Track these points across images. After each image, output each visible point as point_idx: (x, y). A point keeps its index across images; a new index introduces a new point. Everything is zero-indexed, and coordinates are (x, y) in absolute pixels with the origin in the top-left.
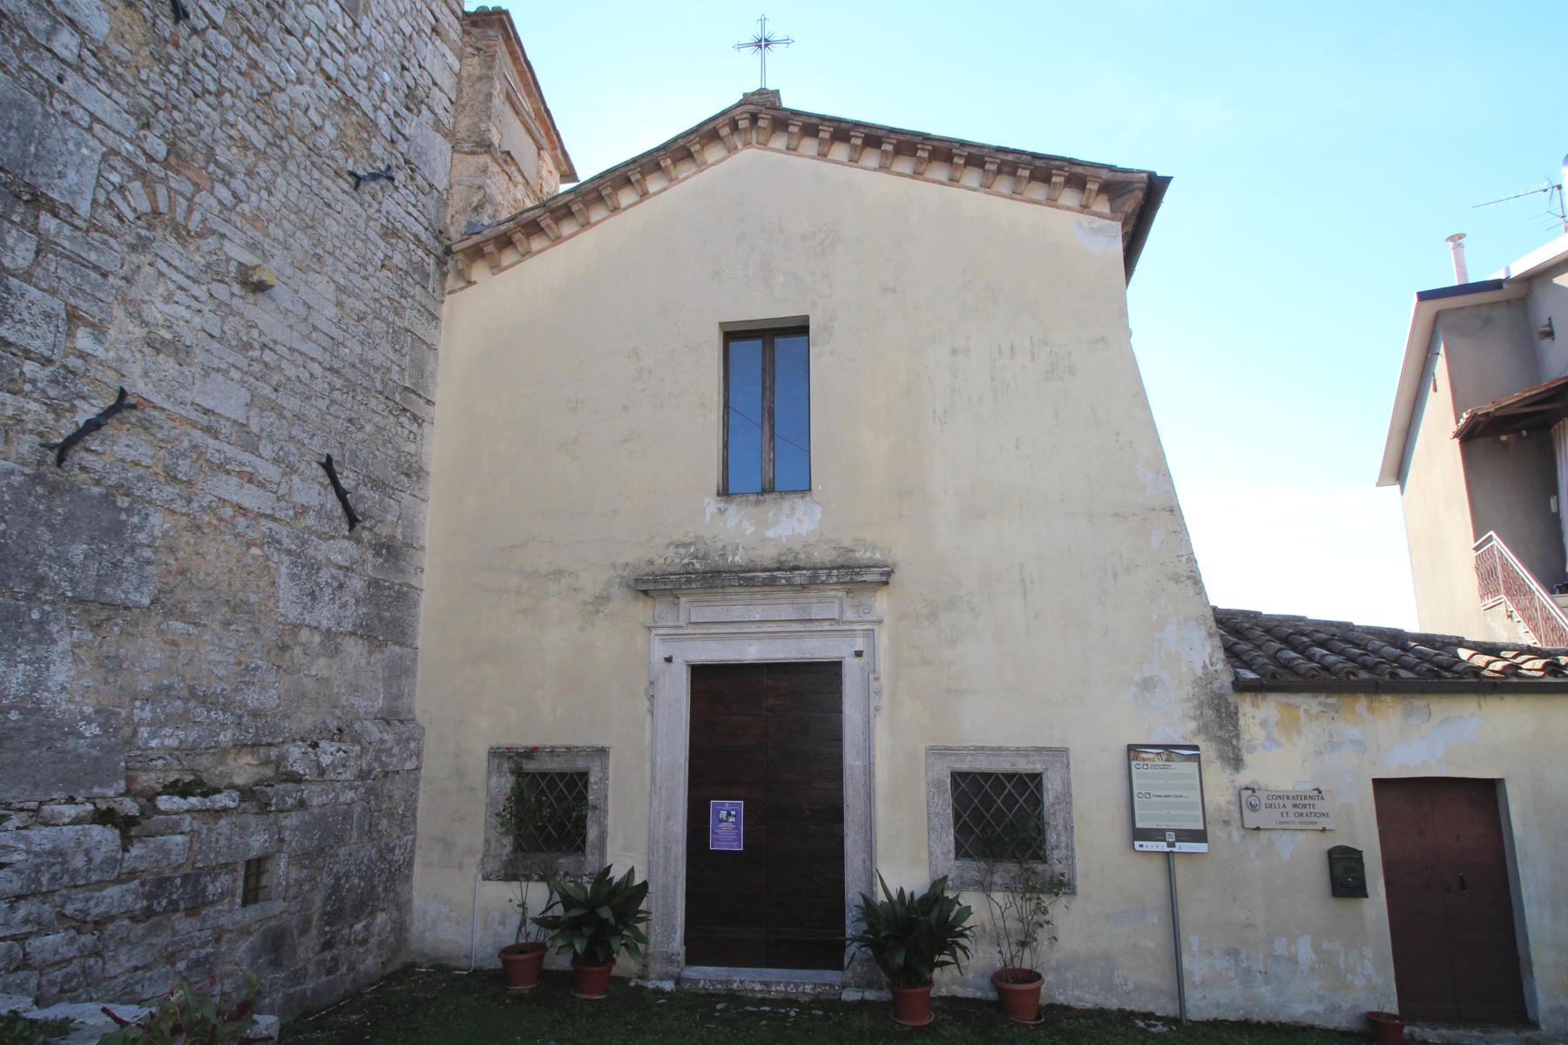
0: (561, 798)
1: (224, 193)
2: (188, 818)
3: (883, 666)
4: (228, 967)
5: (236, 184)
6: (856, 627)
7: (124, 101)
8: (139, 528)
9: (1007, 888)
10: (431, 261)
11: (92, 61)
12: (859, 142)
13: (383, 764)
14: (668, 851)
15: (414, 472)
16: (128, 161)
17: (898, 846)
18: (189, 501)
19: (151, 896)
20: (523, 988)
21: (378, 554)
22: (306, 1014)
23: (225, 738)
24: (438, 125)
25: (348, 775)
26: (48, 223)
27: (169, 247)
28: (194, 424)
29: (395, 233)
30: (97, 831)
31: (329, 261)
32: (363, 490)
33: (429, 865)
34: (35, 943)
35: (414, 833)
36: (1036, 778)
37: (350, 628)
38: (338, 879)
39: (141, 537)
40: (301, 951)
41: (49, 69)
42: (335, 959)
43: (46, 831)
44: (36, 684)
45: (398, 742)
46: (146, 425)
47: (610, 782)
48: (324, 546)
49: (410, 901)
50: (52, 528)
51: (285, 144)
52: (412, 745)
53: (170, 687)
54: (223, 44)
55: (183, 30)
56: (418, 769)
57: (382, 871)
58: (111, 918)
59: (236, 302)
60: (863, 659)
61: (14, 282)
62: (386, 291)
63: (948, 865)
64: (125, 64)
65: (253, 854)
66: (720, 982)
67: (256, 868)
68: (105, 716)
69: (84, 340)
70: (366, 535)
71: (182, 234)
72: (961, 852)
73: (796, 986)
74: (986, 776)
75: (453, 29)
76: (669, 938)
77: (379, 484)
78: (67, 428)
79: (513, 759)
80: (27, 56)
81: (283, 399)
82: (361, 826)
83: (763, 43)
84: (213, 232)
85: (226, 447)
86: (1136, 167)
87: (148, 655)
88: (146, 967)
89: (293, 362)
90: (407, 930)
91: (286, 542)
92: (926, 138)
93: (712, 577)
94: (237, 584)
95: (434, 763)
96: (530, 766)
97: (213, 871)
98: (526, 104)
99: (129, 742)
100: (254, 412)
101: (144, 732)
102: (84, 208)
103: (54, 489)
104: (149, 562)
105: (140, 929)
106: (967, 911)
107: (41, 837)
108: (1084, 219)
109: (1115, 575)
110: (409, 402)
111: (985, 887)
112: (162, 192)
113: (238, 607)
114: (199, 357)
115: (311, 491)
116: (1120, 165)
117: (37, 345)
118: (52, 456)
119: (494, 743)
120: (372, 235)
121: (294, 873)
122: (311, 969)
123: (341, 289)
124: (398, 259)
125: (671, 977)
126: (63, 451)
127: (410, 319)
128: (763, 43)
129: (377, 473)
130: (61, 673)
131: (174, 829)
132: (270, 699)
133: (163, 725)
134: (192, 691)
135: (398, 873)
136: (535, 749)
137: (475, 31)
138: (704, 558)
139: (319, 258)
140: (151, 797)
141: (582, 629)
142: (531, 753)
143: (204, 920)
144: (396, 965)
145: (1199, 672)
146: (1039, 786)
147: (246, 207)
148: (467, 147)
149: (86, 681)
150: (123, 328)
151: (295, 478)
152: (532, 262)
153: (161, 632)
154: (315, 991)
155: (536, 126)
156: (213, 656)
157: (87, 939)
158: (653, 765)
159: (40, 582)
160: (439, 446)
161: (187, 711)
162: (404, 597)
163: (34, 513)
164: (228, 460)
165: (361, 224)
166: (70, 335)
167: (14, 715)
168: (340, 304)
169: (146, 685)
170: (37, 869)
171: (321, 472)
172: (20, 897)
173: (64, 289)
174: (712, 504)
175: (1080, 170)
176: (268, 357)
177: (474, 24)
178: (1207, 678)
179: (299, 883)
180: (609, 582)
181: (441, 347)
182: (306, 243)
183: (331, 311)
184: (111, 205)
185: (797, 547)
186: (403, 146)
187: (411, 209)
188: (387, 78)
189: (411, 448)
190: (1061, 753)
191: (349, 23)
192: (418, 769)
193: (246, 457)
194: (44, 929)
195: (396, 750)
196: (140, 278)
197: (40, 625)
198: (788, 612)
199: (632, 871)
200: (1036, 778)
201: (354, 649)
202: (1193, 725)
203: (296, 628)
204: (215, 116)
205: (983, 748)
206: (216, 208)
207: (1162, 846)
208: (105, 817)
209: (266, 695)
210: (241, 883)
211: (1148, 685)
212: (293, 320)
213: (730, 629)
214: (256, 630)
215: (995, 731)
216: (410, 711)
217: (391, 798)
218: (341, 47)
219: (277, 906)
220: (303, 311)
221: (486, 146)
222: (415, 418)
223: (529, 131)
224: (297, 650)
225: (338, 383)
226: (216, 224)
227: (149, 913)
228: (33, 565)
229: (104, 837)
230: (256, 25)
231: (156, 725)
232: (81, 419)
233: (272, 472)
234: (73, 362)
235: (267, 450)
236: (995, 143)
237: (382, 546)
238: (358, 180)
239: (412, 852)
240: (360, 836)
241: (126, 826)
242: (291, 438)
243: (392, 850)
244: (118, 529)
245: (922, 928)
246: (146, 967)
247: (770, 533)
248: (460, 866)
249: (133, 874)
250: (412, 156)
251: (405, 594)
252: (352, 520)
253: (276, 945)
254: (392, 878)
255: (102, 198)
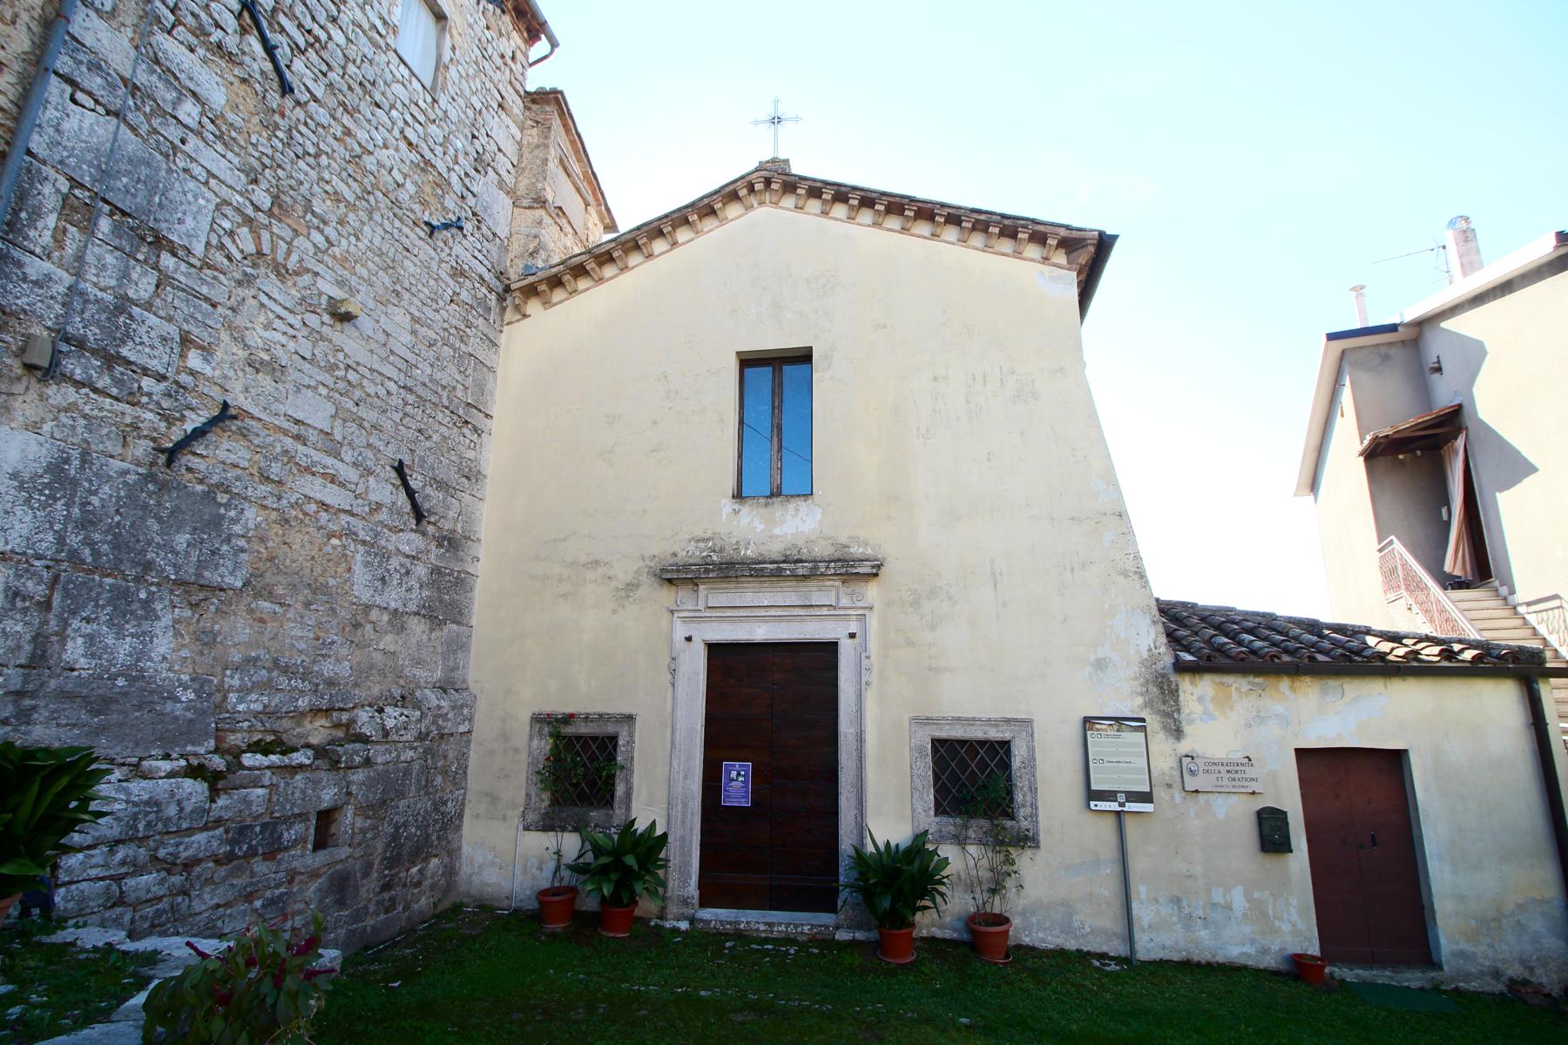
0: (593, 758)
1: (317, 238)
2: (268, 773)
3: (873, 646)
4: (301, 906)
5: (329, 231)
6: (850, 612)
7: (236, 160)
8: (235, 521)
9: (980, 842)
10: (493, 297)
11: (211, 127)
12: (856, 202)
13: (439, 727)
14: (685, 805)
15: (472, 475)
16: (238, 210)
17: (886, 804)
18: (280, 498)
19: (233, 842)
20: (557, 927)
21: (440, 545)
22: (367, 948)
23: (303, 703)
24: (501, 184)
25: (409, 737)
26: (167, 261)
27: (270, 283)
28: (286, 432)
29: (462, 274)
30: (189, 784)
31: (406, 295)
32: (428, 490)
33: (478, 816)
34: (130, 882)
35: (465, 788)
36: (1005, 745)
37: (414, 609)
38: (397, 828)
39: (237, 529)
40: (363, 893)
41: (174, 133)
42: (392, 899)
43: (144, 783)
44: (140, 655)
45: (453, 708)
46: (244, 434)
47: (636, 745)
48: (394, 538)
49: (460, 848)
50: (160, 520)
51: (371, 198)
52: (465, 711)
53: (257, 659)
54: (322, 115)
55: (288, 102)
56: (470, 732)
57: (436, 821)
58: (197, 861)
59: (326, 330)
60: (856, 641)
61: (136, 310)
62: (454, 322)
63: (929, 821)
64: (239, 131)
65: (324, 805)
66: (730, 923)
67: (326, 818)
68: (199, 683)
69: (194, 360)
70: (430, 529)
71: (281, 271)
72: (940, 810)
73: (796, 926)
74: (962, 742)
75: (515, 104)
76: (685, 883)
77: (442, 485)
78: (177, 434)
79: (553, 724)
80: (156, 122)
81: (363, 412)
82: (419, 781)
83: (776, 120)
84: (308, 271)
85: (312, 452)
86: (1088, 227)
87: (238, 631)
88: (228, 905)
89: (372, 381)
90: (456, 874)
91: (362, 534)
92: (912, 200)
93: (729, 569)
94: (318, 570)
95: (484, 726)
96: (568, 730)
97: (288, 820)
98: (576, 168)
99: (219, 707)
100: (338, 422)
101: (233, 697)
102: (199, 249)
103: (164, 487)
104: (243, 550)
105: (223, 871)
106: (945, 862)
107: (140, 789)
108: (1046, 268)
109: (1072, 570)
110: (469, 416)
111: (960, 840)
112: (265, 236)
113: (318, 589)
114: (293, 375)
115: (385, 491)
116: (1075, 224)
117: (155, 365)
118: (162, 459)
119: (537, 710)
120: (443, 275)
121: (359, 822)
122: (372, 908)
123: (415, 320)
124: (465, 296)
125: (686, 918)
126: (172, 454)
127: (474, 345)
128: (776, 120)
129: (441, 476)
130: (163, 645)
131: (256, 783)
132: (344, 670)
133: (249, 691)
134: (276, 662)
135: (450, 823)
136: (572, 716)
137: (534, 107)
138: (721, 550)
139: (398, 294)
140: (237, 753)
141: (614, 612)
142: (569, 718)
143: (279, 863)
144: (447, 904)
145: (1145, 655)
146: (1008, 752)
147: (336, 250)
148: (525, 203)
149: (185, 653)
150: (227, 349)
151: (371, 479)
152: (577, 299)
153: (251, 611)
154: (374, 928)
155: (584, 186)
156: (296, 633)
157: (177, 880)
158: (673, 732)
159: (148, 566)
160: (496, 453)
161: (270, 680)
162: (461, 582)
163: (145, 506)
164: (314, 464)
165: (434, 265)
166: (183, 356)
167: (121, 682)
168: (414, 333)
169: (237, 657)
170: (135, 817)
171: (394, 474)
172: (118, 842)
173: (179, 316)
174: (728, 505)
175: (1041, 228)
176: (352, 376)
177: (534, 101)
178: (1152, 659)
179: (363, 831)
180: (638, 572)
181: (499, 370)
182: (387, 280)
183: (407, 338)
184: (222, 247)
185: (800, 543)
186: (471, 201)
187: (476, 253)
188: (459, 145)
189: (471, 454)
190: (1027, 723)
191: (429, 99)
192: (470, 732)
193: (330, 461)
194: (139, 870)
195: (451, 715)
196: (244, 309)
197: (146, 604)
198: (792, 599)
199: (654, 822)
200: (1005, 745)
201: (417, 627)
202: (1140, 700)
203: (368, 608)
204: (313, 174)
205: (959, 719)
206: (312, 250)
207: (1114, 806)
208: (196, 772)
209: (337, 668)
210: (312, 831)
211: (1101, 665)
212: (373, 345)
213: (742, 613)
214: (333, 609)
215: (971, 703)
216: (464, 681)
217: (445, 757)
218: (422, 118)
219: (344, 852)
220: (382, 338)
221: (541, 202)
222: (475, 429)
223: (578, 190)
224: (369, 627)
225: (411, 398)
226: (311, 264)
227: (231, 857)
228: (143, 552)
229: (195, 789)
230: (351, 100)
231: (244, 691)
232: (189, 427)
233: (352, 475)
234: (184, 378)
235: (348, 455)
236: (971, 206)
237: (444, 538)
238: (432, 229)
239: (463, 804)
240: (418, 791)
241: (215, 781)
242: (369, 445)
243: (445, 803)
244: (216, 522)
245: (906, 876)
246: (228, 905)
247: (777, 531)
248: (504, 818)
249: (218, 822)
250: (478, 210)
251: (463, 580)
252: (419, 514)
253: (341, 886)
254: (444, 828)
255: (214, 241)
